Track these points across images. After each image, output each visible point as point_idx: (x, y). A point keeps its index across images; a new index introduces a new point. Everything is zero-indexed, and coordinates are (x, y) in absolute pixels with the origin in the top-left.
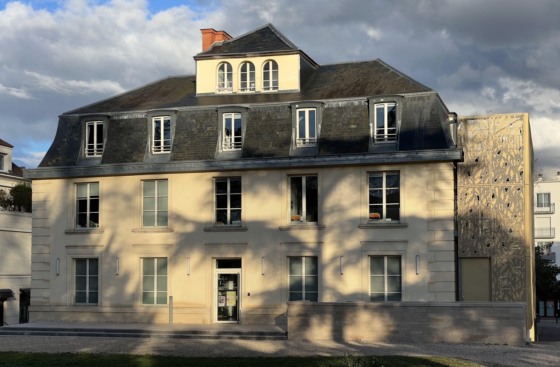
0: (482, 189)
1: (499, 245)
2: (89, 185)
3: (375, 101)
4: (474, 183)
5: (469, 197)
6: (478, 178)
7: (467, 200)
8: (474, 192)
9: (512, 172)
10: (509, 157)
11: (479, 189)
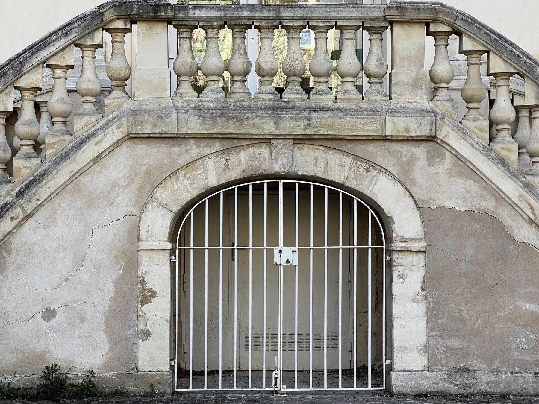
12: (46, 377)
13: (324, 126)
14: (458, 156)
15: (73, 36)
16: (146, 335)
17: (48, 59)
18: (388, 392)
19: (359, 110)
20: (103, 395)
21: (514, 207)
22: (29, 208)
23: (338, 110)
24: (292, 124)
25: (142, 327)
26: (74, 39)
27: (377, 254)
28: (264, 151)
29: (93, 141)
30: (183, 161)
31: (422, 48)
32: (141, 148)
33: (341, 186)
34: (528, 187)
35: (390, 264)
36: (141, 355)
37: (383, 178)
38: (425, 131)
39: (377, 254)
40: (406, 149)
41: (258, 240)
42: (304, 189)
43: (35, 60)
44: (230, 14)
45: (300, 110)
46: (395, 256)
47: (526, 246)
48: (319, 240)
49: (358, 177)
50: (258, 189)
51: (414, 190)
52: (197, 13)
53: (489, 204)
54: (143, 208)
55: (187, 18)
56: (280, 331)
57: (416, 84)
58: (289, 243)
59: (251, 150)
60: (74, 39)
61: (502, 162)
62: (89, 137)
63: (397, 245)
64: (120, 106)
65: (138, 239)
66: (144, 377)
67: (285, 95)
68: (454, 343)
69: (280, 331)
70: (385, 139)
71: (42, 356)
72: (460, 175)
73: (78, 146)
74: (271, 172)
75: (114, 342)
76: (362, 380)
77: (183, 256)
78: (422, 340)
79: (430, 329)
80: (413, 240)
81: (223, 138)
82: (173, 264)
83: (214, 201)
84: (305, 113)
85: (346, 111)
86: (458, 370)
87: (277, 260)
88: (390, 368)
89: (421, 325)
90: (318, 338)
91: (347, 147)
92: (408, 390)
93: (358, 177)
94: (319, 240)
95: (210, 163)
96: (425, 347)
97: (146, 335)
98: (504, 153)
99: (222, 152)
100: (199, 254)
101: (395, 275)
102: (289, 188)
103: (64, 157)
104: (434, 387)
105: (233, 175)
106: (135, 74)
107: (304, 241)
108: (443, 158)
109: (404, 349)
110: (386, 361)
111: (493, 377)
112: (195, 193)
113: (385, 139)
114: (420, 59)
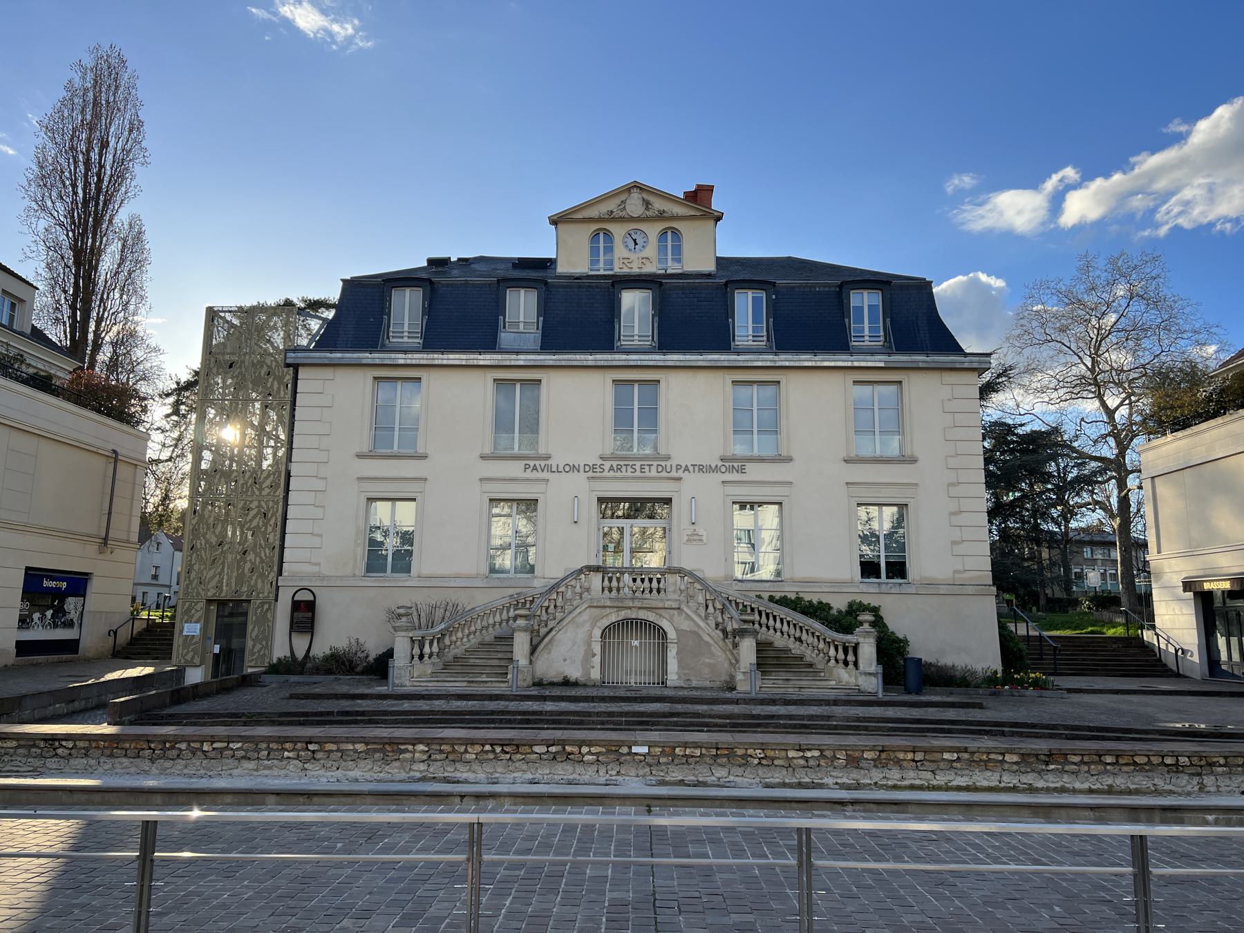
0: (249, 494)
1: (250, 481)
2: (636, 387)
3: (267, 38)
4: (259, 501)
5: (252, 513)
6: (267, 487)
7: (249, 517)
8: (261, 490)
9: (276, 383)
10: (258, 560)
11: (253, 492)
14: (687, 614)
16: (593, 667)
17: (495, 744)
18: (666, 687)
21: (704, 630)
26: (694, 693)
27: (663, 643)
28: (629, 611)
31: (676, 581)
32: (593, 610)
34: (707, 624)
37: (665, 620)
38: (677, 606)
39: (663, 643)
40: (671, 611)
53: (696, 629)
54: (593, 629)
57: (674, 592)
58: (637, 640)
60: (694, 693)
61: (700, 616)
66: (593, 680)
68: (686, 672)
70: (665, 608)
75: (583, 669)
76: (658, 684)
77: (605, 643)
79: (678, 667)
81: (617, 607)
90: (645, 671)
94: (641, 639)
97: (593, 667)
103: (570, 613)
105: (620, 618)
106: (592, 587)
107: (641, 639)
113: (665, 608)
114: (675, 583)
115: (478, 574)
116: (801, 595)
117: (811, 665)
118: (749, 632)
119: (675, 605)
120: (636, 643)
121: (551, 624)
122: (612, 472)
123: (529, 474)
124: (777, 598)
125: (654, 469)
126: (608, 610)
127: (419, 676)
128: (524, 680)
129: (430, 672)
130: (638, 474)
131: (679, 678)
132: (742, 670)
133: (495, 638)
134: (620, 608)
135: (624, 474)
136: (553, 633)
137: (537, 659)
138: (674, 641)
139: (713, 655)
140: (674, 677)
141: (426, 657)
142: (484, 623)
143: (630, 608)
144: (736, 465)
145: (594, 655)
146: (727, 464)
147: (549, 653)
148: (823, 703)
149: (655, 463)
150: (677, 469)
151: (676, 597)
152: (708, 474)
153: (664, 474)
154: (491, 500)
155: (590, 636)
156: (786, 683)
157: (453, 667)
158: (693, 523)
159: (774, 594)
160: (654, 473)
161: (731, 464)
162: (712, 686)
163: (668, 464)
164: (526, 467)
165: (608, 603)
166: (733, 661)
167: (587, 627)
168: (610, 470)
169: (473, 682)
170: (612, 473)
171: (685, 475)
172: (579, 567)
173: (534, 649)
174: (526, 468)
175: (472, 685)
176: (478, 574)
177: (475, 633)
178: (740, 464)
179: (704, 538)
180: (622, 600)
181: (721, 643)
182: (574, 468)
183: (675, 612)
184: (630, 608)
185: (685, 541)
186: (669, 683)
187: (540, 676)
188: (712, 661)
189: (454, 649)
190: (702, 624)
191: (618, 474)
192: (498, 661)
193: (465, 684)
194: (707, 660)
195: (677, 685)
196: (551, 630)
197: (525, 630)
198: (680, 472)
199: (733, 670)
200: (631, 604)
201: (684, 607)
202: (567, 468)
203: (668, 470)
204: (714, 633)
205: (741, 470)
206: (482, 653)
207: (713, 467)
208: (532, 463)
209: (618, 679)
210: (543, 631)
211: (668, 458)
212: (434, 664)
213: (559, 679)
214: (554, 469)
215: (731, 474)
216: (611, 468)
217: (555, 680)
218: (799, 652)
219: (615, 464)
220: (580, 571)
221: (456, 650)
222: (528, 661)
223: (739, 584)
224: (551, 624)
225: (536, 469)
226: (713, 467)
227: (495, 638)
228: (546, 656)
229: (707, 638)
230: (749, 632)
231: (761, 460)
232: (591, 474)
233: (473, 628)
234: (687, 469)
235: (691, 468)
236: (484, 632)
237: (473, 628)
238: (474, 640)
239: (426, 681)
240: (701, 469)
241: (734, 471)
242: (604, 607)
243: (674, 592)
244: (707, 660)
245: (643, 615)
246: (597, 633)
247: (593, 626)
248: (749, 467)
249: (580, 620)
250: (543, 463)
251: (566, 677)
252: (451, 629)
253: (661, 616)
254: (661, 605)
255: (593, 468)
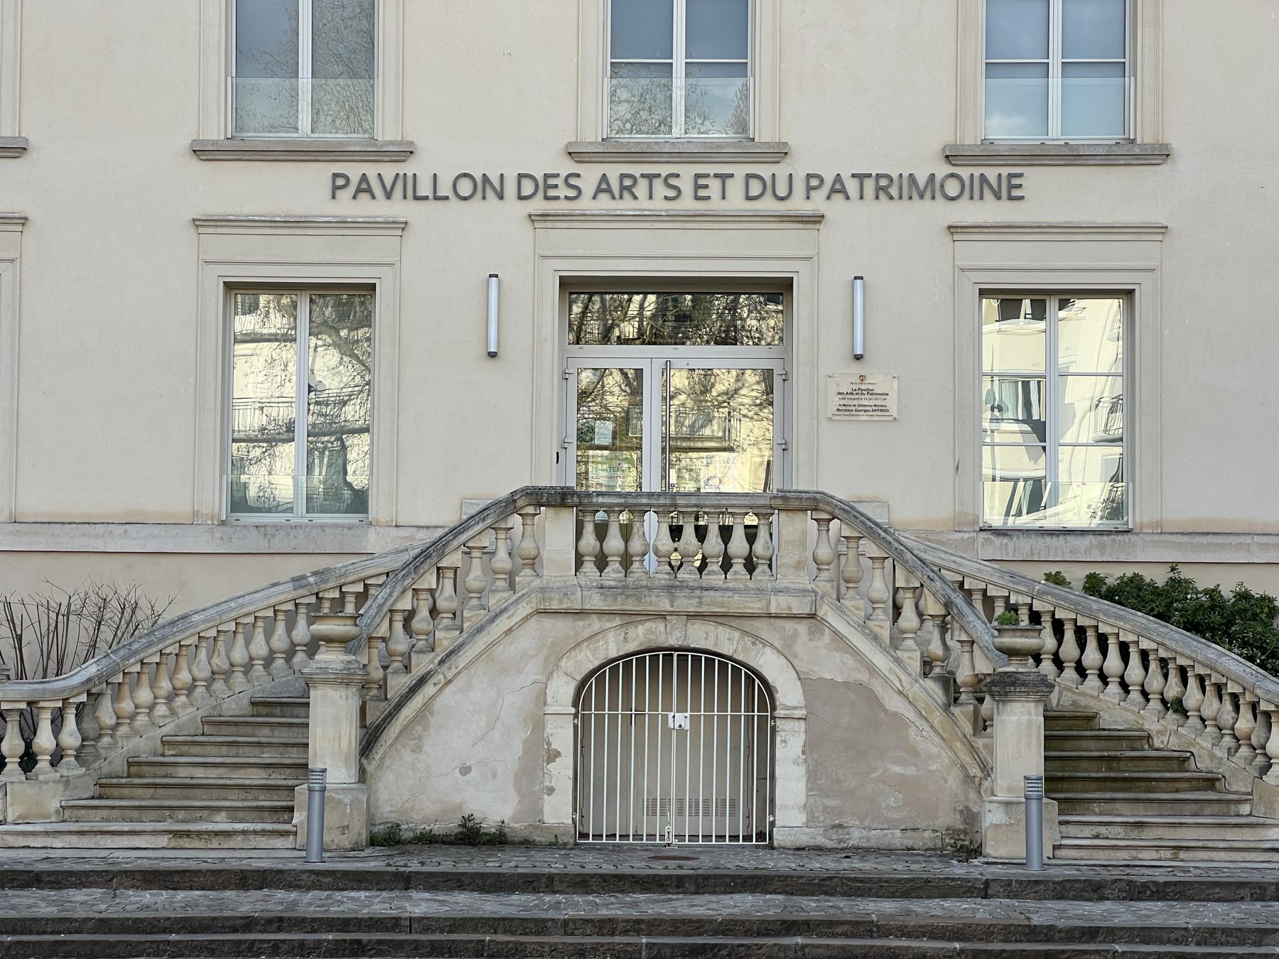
12: (464, 826)
13: (714, 604)
14: (835, 632)
15: (489, 521)
16: (551, 791)
19: (747, 589)
20: (513, 843)
21: (885, 679)
22: (450, 675)
23: (727, 589)
24: (686, 601)
25: (547, 783)
28: (659, 626)
29: (505, 615)
30: (586, 634)
31: (805, 533)
32: (548, 622)
33: (731, 659)
34: (898, 661)
35: (774, 729)
36: (546, 809)
37: (768, 650)
38: (806, 610)
40: (789, 625)
41: (654, 706)
42: (696, 660)
43: (456, 543)
44: (630, 501)
45: (693, 589)
46: (778, 722)
47: (895, 714)
48: (723, 707)
49: (745, 650)
50: (654, 659)
51: (796, 663)
52: (600, 500)
53: (864, 677)
54: (549, 677)
55: (591, 504)
56: (673, 796)
57: (799, 566)
58: (682, 709)
59: (648, 625)
61: (875, 638)
62: (502, 612)
63: (779, 712)
64: (529, 584)
65: (545, 704)
67: (681, 575)
68: (831, 803)
69: (673, 796)
70: (770, 616)
71: (459, 807)
72: (838, 650)
73: (492, 620)
74: (666, 645)
77: (586, 719)
78: (802, 798)
79: (809, 790)
80: (795, 708)
81: (623, 614)
82: (576, 727)
83: (614, 671)
84: (698, 592)
85: (734, 590)
86: (834, 827)
87: (671, 725)
88: (773, 824)
89: (802, 786)
91: (735, 623)
92: (788, 844)
93: (745, 650)
94: (709, 707)
95: (611, 635)
96: (805, 806)
98: (877, 630)
99: (622, 626)
100: (600, 719)
101: (778, 739)
102: (682, 659)
103: (480, 629)
104: (811, 842)
105: (631, 647)
107: (696, 707)
108: (822, 633)
109: (785, 807)
110: (769, 818)
111: (865, 833)
112: (597, 663)
113: (770, 616)
115: (195, 514)
116: (1185, 573)
117: (1210, 782)
118: (1024, 684)
119: (800, 606)
120: (680, 719)
121: (422, 664)
122: (604, 199)
123: (346, 206)
124: (1111, 581)
125: (735, 188)
126: (596, 624)
127: (24, 819)
128: (344, 829)
129: (55, 804)
130: (687, 203)
131: (811, 821)
132: (1002, 796)
133: (253, 704)
134: (630, 617)
135: (643, 204)
136: (429, 690)
137: (380, 766)
138: (798, 713)
139: (915, 753)
140: (798, 818)
141: (43, 763)
142: (220, 662)
143: (662, 616)
144: (991, 174)
145: (553, 756)
146: (965, 173)
147: (417, 749)
148: (1245, 892)
149: (740, 171)
150: (809, 189)
151: (803, 581)
152: (905, 204)
153: (768, 204)
154: (230, 287)
155: (542, 699)
156: (1135, 834)
157: (126, 791)
158: (858, 358)
159: (1101, 571)
160: (735, 201)
161: (977, 172)
162: (909, 843)
163: (781, 171)
164: (338, 184)
165: (596, 602)
166: (975, 771)
167: (532, 672)
168: (599, 190)
169: (188, 834)
170: (605, 203)
171: (835, 209)
172: (504, 493)
173: (370, 739)
174: (335, 188)
175: (185, 842)
176: (195, 514)
177: (191, 689)
178: (1005, 171)
179: (892, 404)
180: (637, 591)
181: (938, 717)
182: (486, 187)
183: (802, 627)
184: (662, 616)
185: (832, 409)
186: (779, 837)
187: (393, 818)
188: (911, 771)
189: (128, 737)
190: (881, 661)
191: (627, 205)
192: (262, 773)
193: (164, 841)
194: (897, 769)
195: (804, 840)
196: (422, 681)
197: (343, 680)
198: (819, 196)
199: (973, 795)
200: (665, 605)
201: (827, 612)
202: (465, 188)
203: (782, 192)
204: (916, 687)
205: (1009, 191)
206: (212, 750)
207: (922, 181)
208: (354, 171)
209: (611, 824)
210: (398, 684)
211: (779, 153)
212: (66, 782)
213: (448, 825)
214: (425, 189)
215: (977, 203)
216: (603, 187)
217: (438, 828)
218: (1174, 743)
219: (613, 172)
220: (509, 505)
221: (136, 741)
222: (354, 771)
223: (998, 541)
224: (422, 664)
225: (369, 190)
226: (922, 181)
227: (253, 704)
228: (407, 756)
229: (894, 704)
230: (1024, 684)
231: (1071, 157)
232: (538, 205)
233: (184, 677)
234: (838, 188)
235: (852, 186)
236: (219, 686)
237: (184, 677)
238: (189, 713)
239: (47, 833)
240: (884, 186)
241: (987, 192)
242: (582, 613)
243: (799, 566)
244: (897, 769)
245: (701, 636)
246: (562, 691)
247: (551, 667)
248: (1035, 179)
249: (510, 650)
250: (389, 171)
251: (470, 818)
252: (119, 678)
253: (756, 638)
254: (755, 606)
255: (545, 186)
